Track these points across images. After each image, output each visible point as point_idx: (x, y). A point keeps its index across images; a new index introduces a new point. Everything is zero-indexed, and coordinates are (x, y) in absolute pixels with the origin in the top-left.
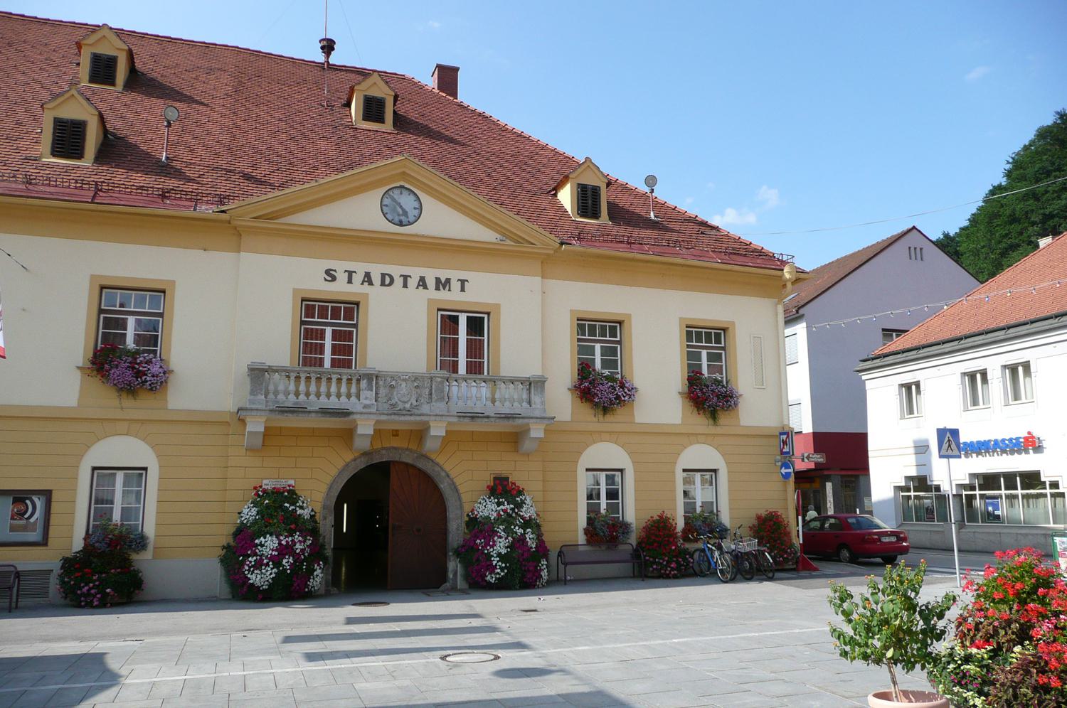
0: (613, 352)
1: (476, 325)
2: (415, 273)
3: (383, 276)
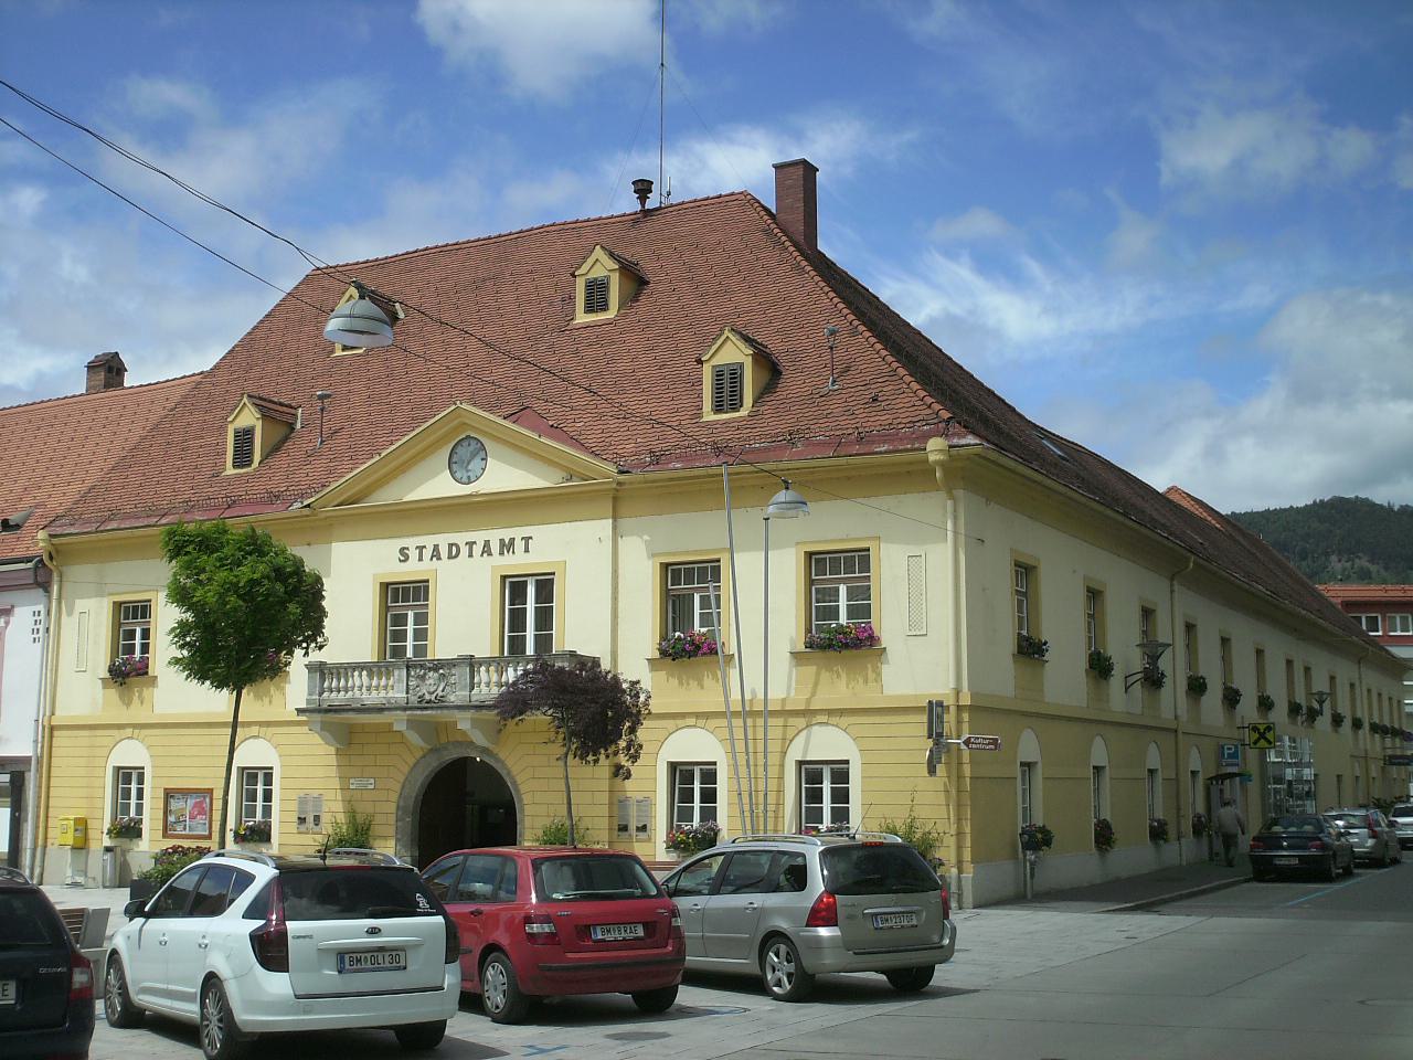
3: (451, 545)
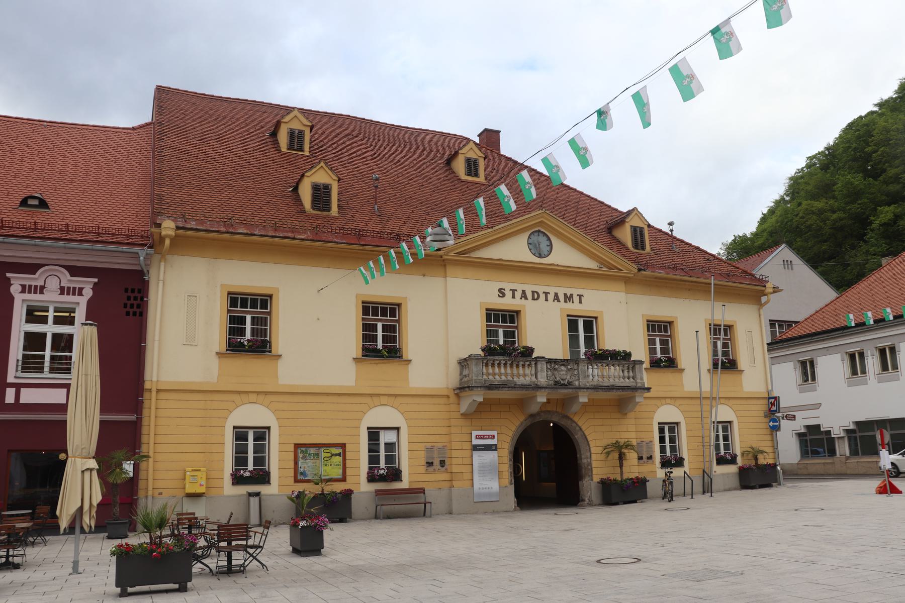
0: (264, 321)
1: (588, 326)
2: (552, 291)
3: (533, 292)
